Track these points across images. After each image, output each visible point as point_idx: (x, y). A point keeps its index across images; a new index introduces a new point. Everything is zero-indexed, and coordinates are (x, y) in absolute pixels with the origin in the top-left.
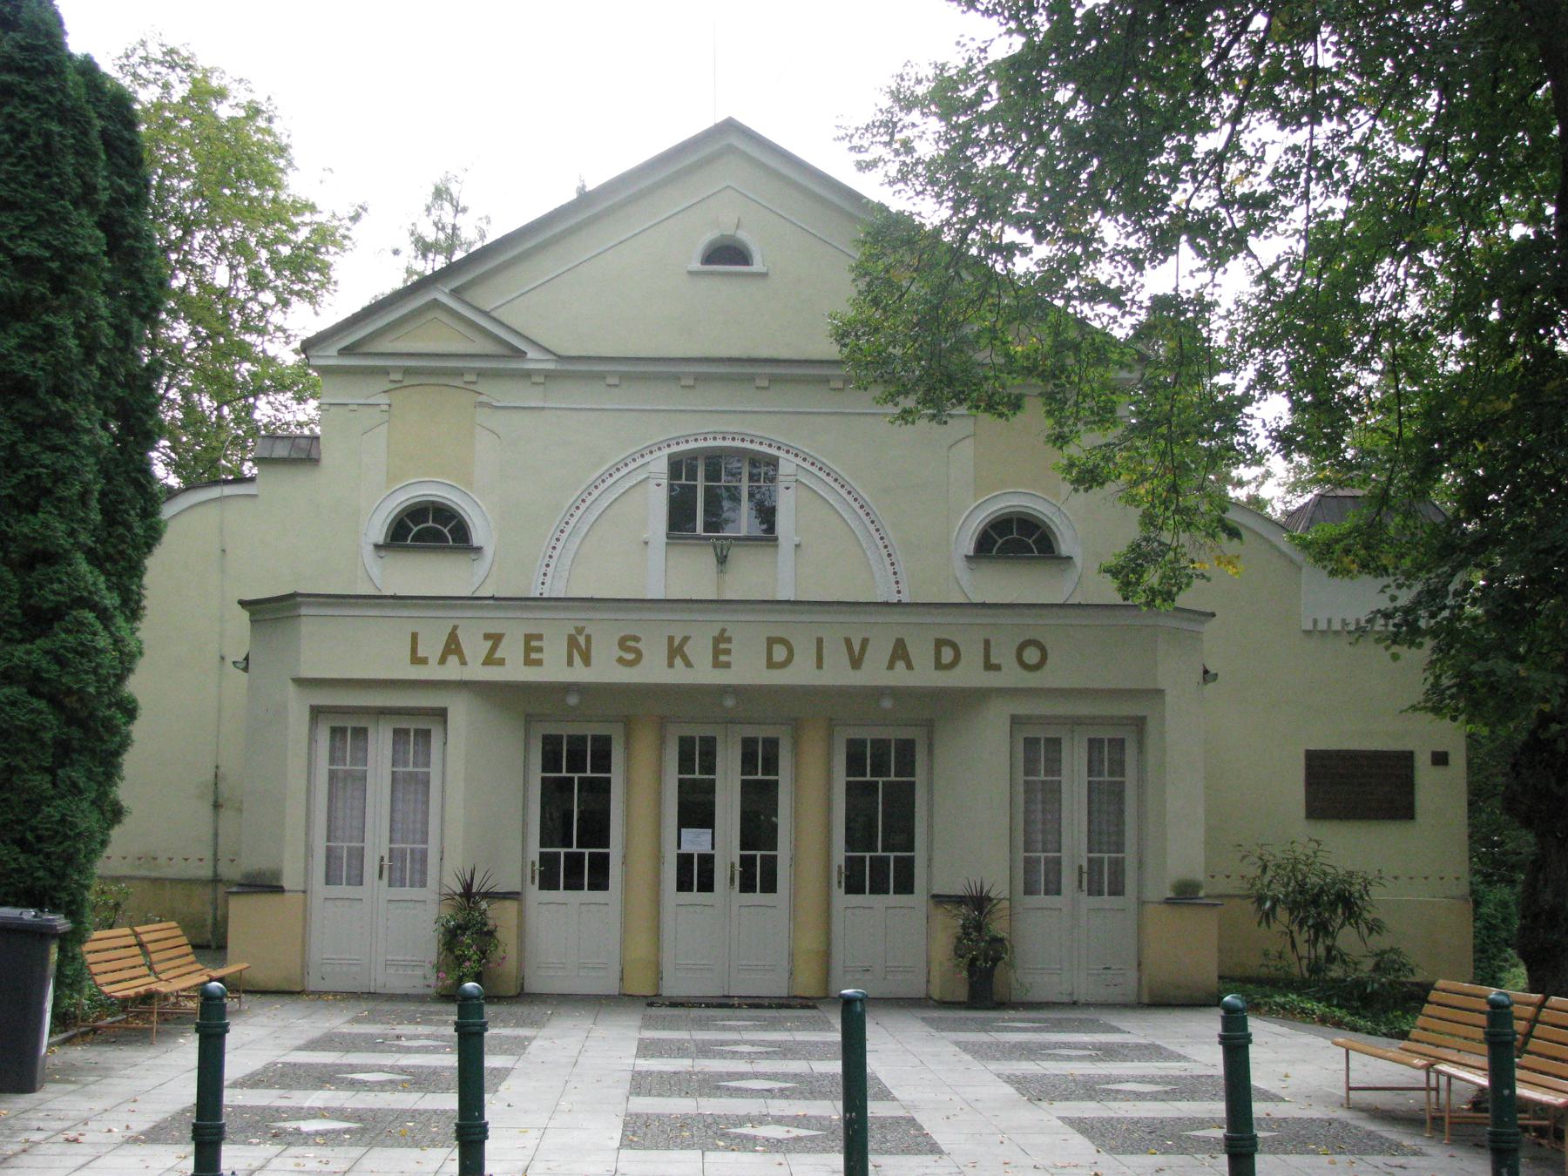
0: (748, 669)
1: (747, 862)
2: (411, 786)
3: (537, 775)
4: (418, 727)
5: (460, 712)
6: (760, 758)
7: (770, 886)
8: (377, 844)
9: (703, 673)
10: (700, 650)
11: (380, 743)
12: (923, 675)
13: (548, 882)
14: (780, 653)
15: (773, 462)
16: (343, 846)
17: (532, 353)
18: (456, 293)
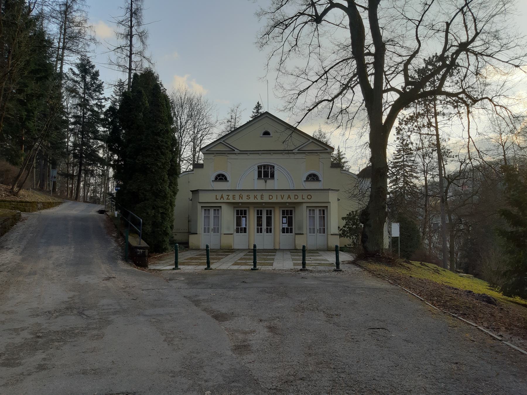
0: (266, 200)
1: (267, 228)
2: (217, 218)
3: (236, 216)
4: (217, 209)
5: (224, 208)
6: (269, 213)
7: (271, 232)
8: (212, 227)
9: (259, 200)
10: (259, 197)
11: (212, 211)
12: (293, 200)
13: (237, 232)
14: (271, 197)
15: (274, 167)
16: (207, 227)
17: (236, 150)
18: (223, 141)
